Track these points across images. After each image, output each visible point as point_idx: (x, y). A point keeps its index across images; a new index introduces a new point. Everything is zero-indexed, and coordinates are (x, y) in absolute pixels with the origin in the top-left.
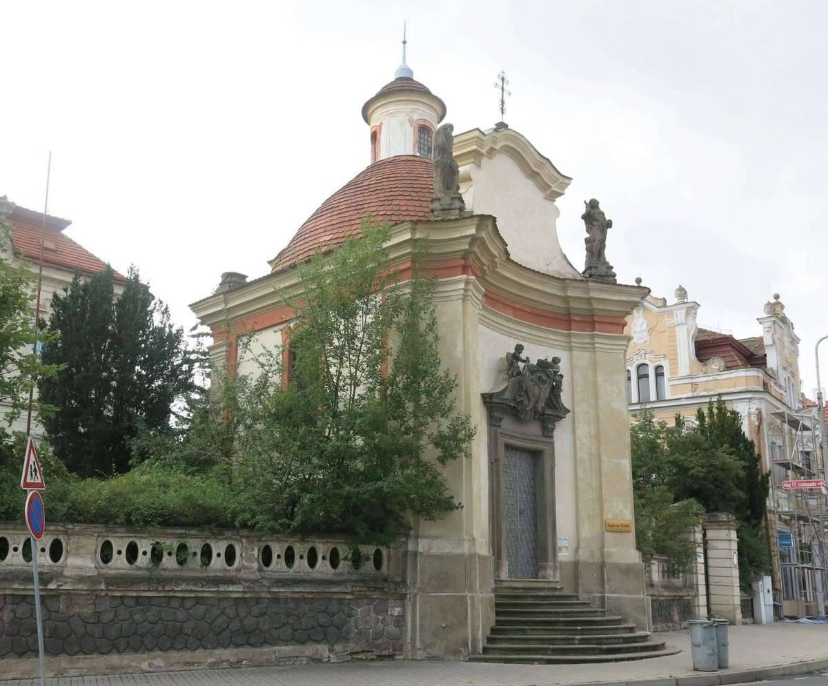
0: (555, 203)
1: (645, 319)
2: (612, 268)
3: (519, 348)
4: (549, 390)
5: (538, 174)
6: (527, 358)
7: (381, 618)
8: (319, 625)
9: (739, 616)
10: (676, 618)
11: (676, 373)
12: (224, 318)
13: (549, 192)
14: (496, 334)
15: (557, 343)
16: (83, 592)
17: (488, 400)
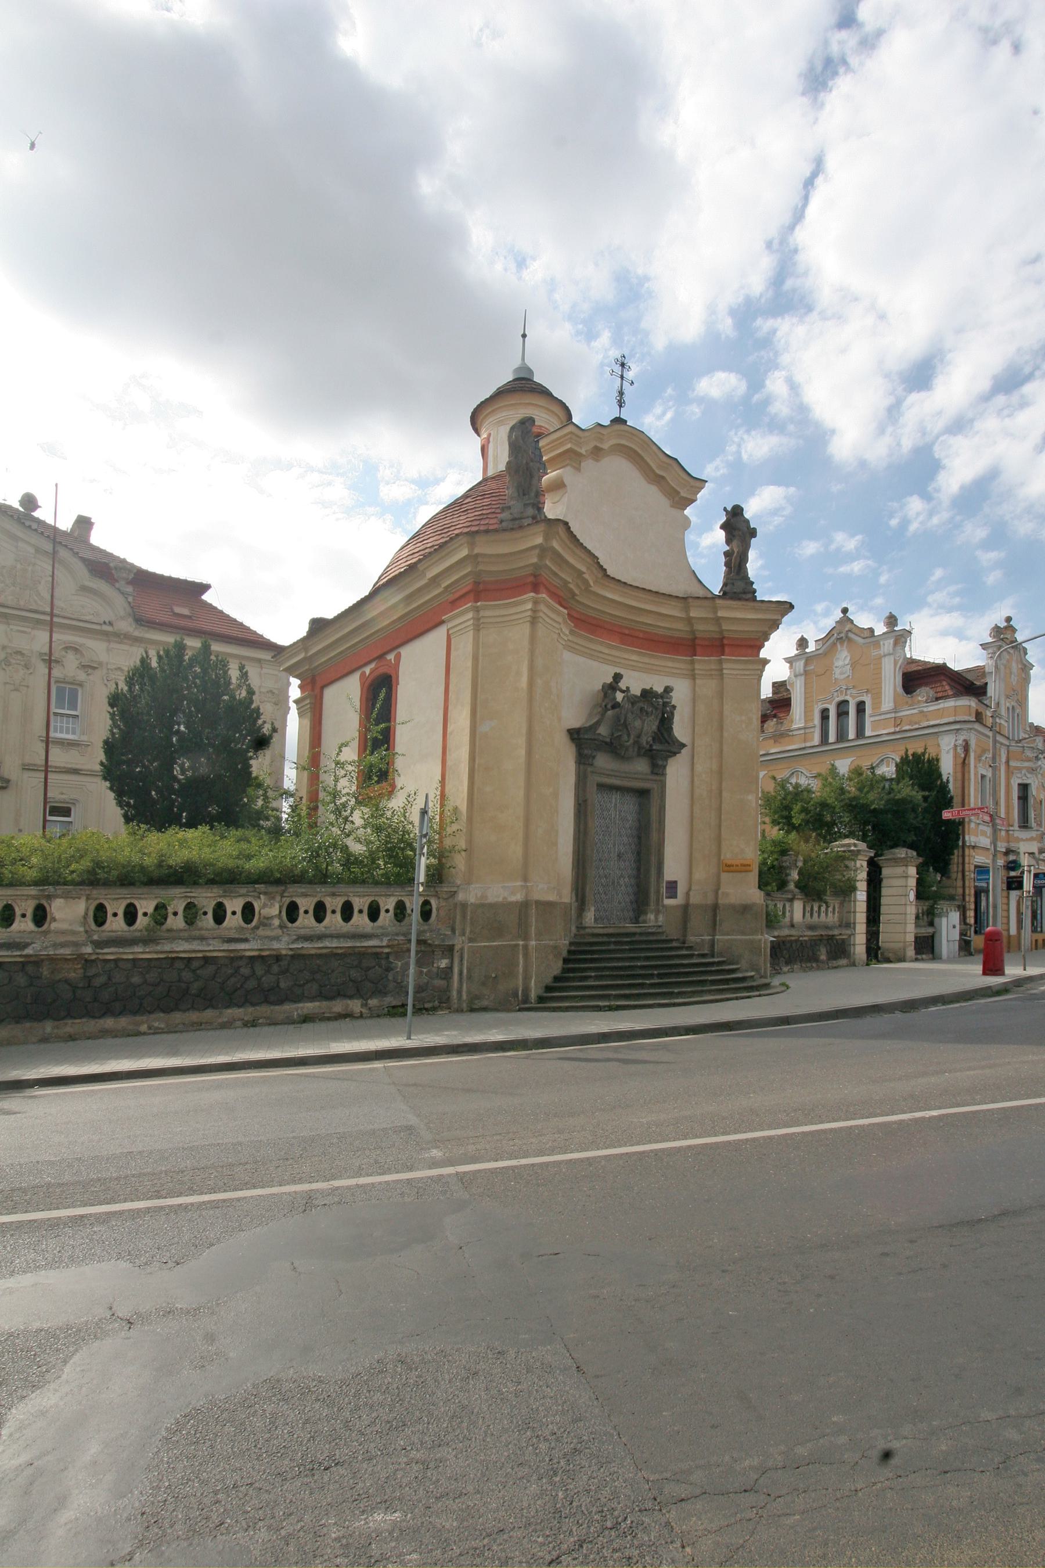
0: (686, 512)
1: (848, 652)
2: (753, 583)
3: (617, 677)
4: (657, 723)
5: (663, 478)
6: (628, 688)
7: (425, 970)
8: (351, 980)
9: (911, 952)
10: (823, 957)
11: (880, 708)
12: (307, 667)
13: (677, 499)
14: (595, 664)
15: (675, 671)
16: (69, 957)
17: (576, 736)
